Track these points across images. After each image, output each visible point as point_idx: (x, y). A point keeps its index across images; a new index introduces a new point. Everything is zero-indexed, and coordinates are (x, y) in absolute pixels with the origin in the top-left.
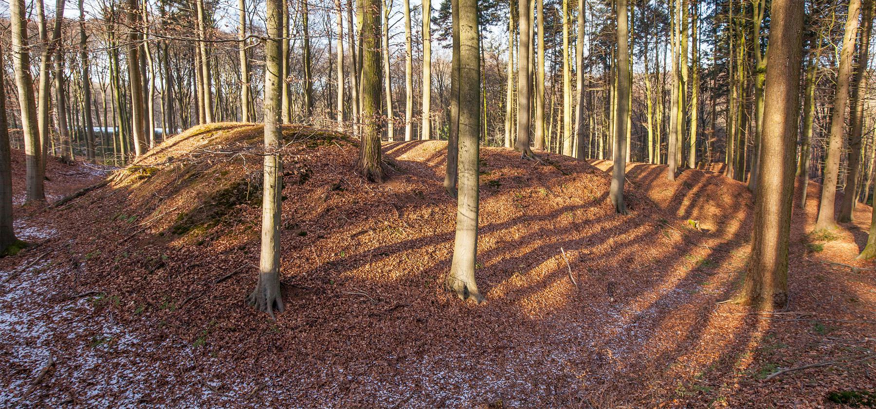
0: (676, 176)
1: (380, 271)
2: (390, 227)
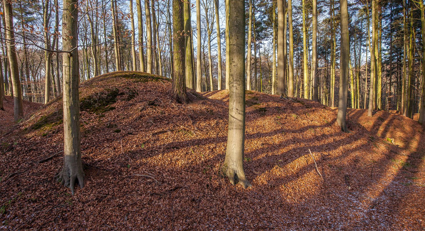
0: (373, 114)
1: (169, 160)
2: (185, 130)
